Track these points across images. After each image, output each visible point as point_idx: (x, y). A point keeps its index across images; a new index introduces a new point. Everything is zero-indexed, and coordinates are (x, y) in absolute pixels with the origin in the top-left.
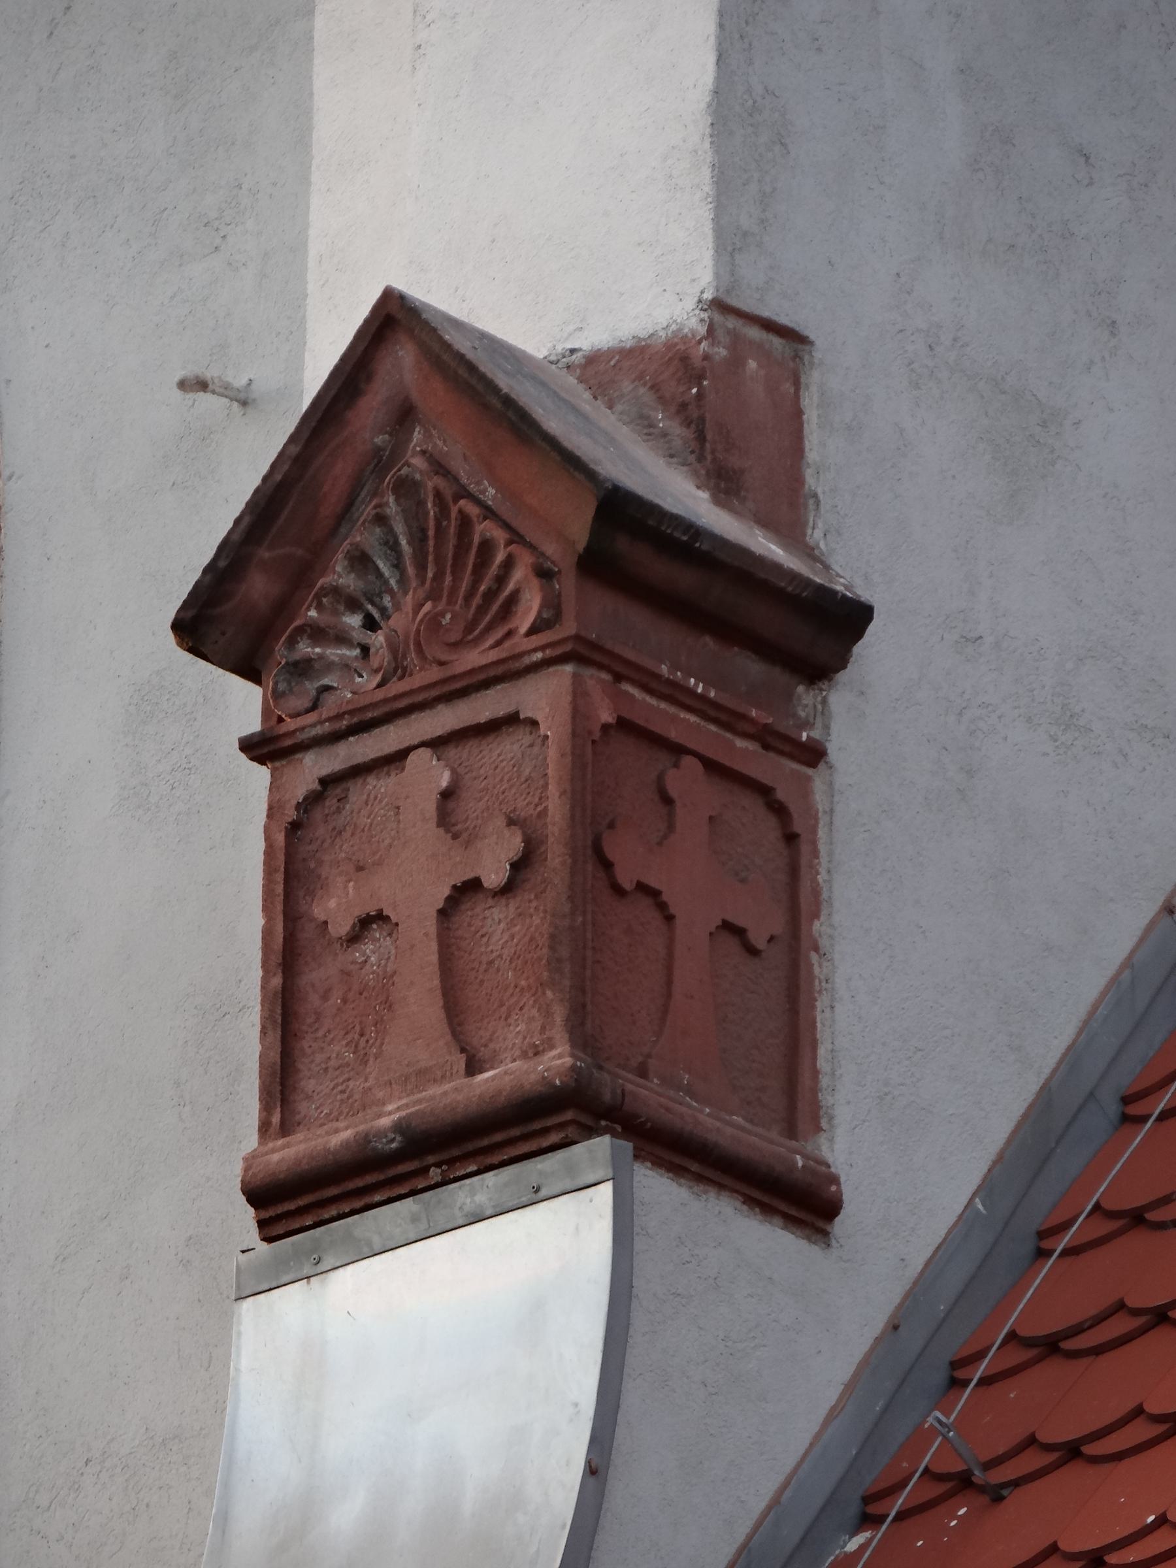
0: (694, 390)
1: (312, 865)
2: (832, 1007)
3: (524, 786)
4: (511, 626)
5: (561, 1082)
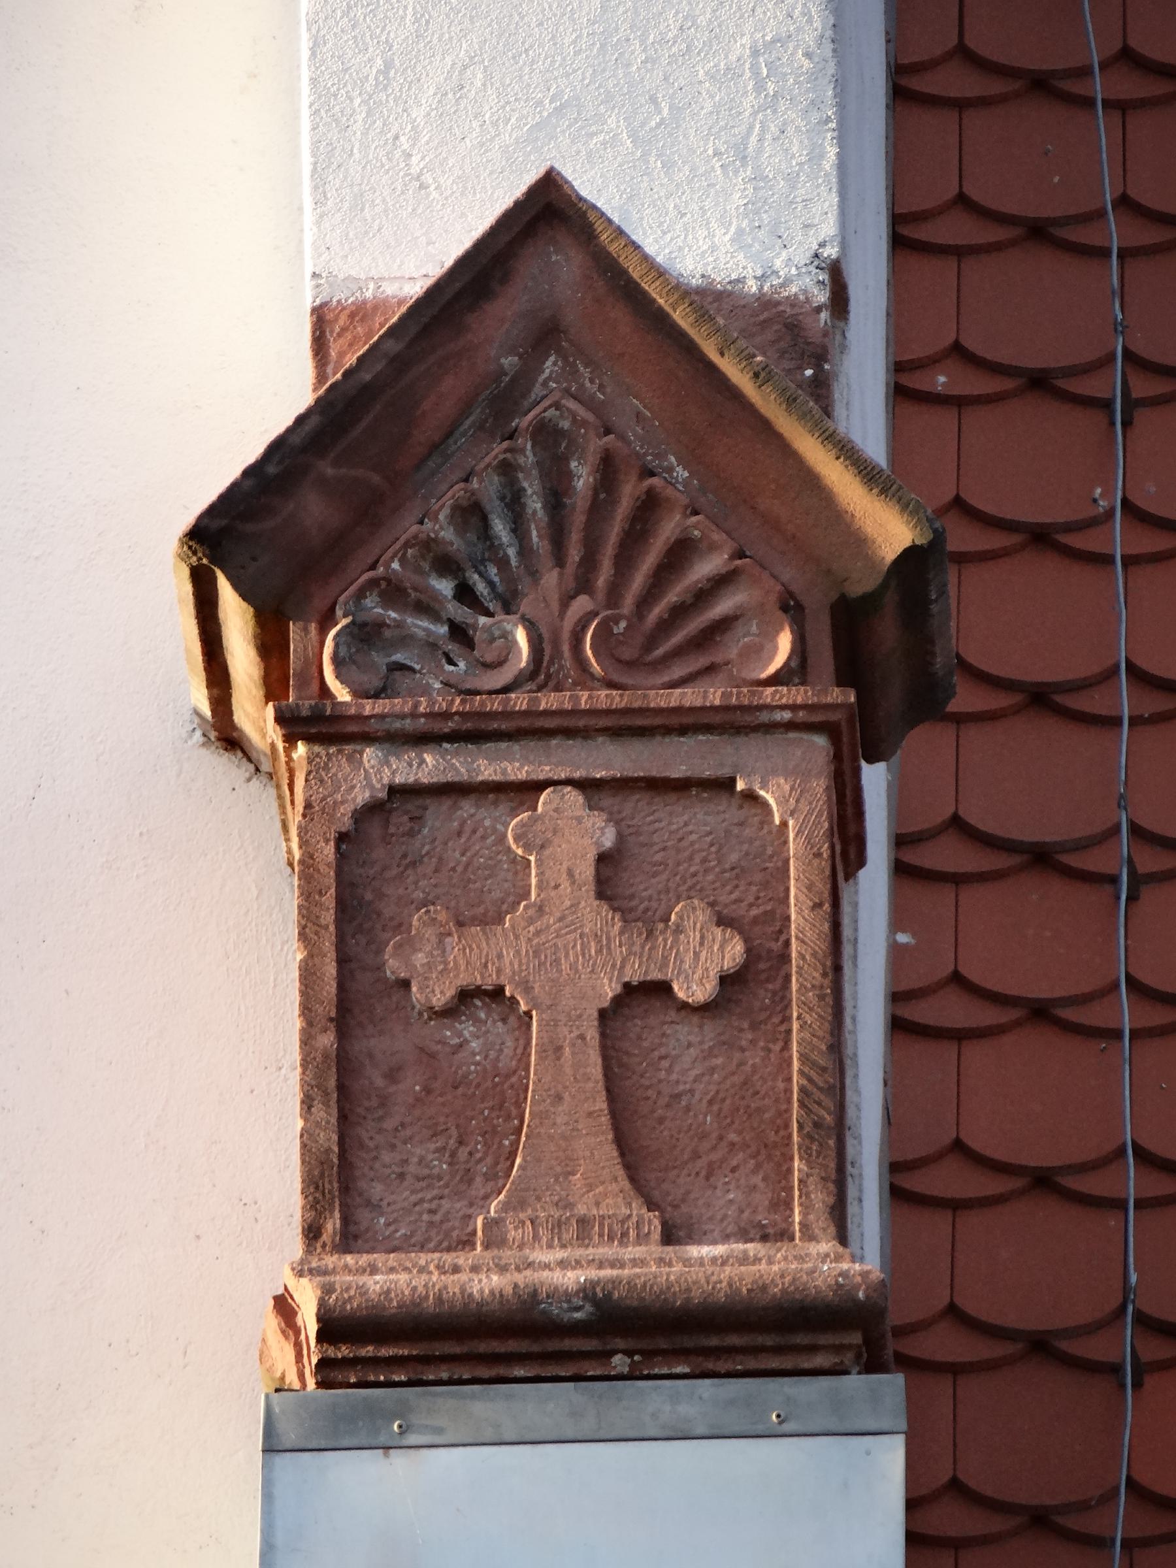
0: (809, 372)
1: (369, 896)
2: (860, 1200)
3: (727, 875)
4: (718, 658)
5: (867, 1297)
